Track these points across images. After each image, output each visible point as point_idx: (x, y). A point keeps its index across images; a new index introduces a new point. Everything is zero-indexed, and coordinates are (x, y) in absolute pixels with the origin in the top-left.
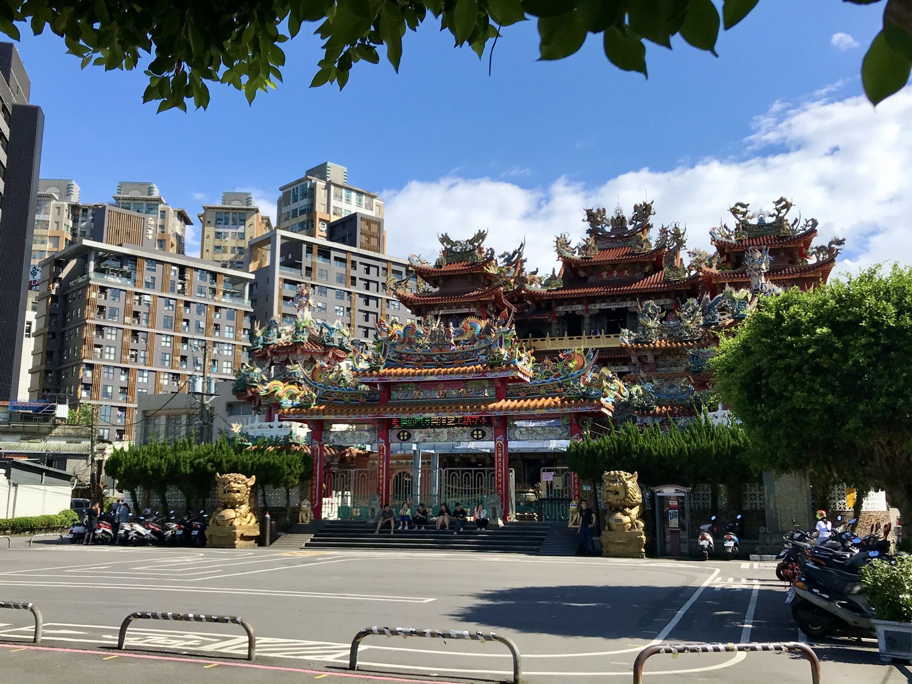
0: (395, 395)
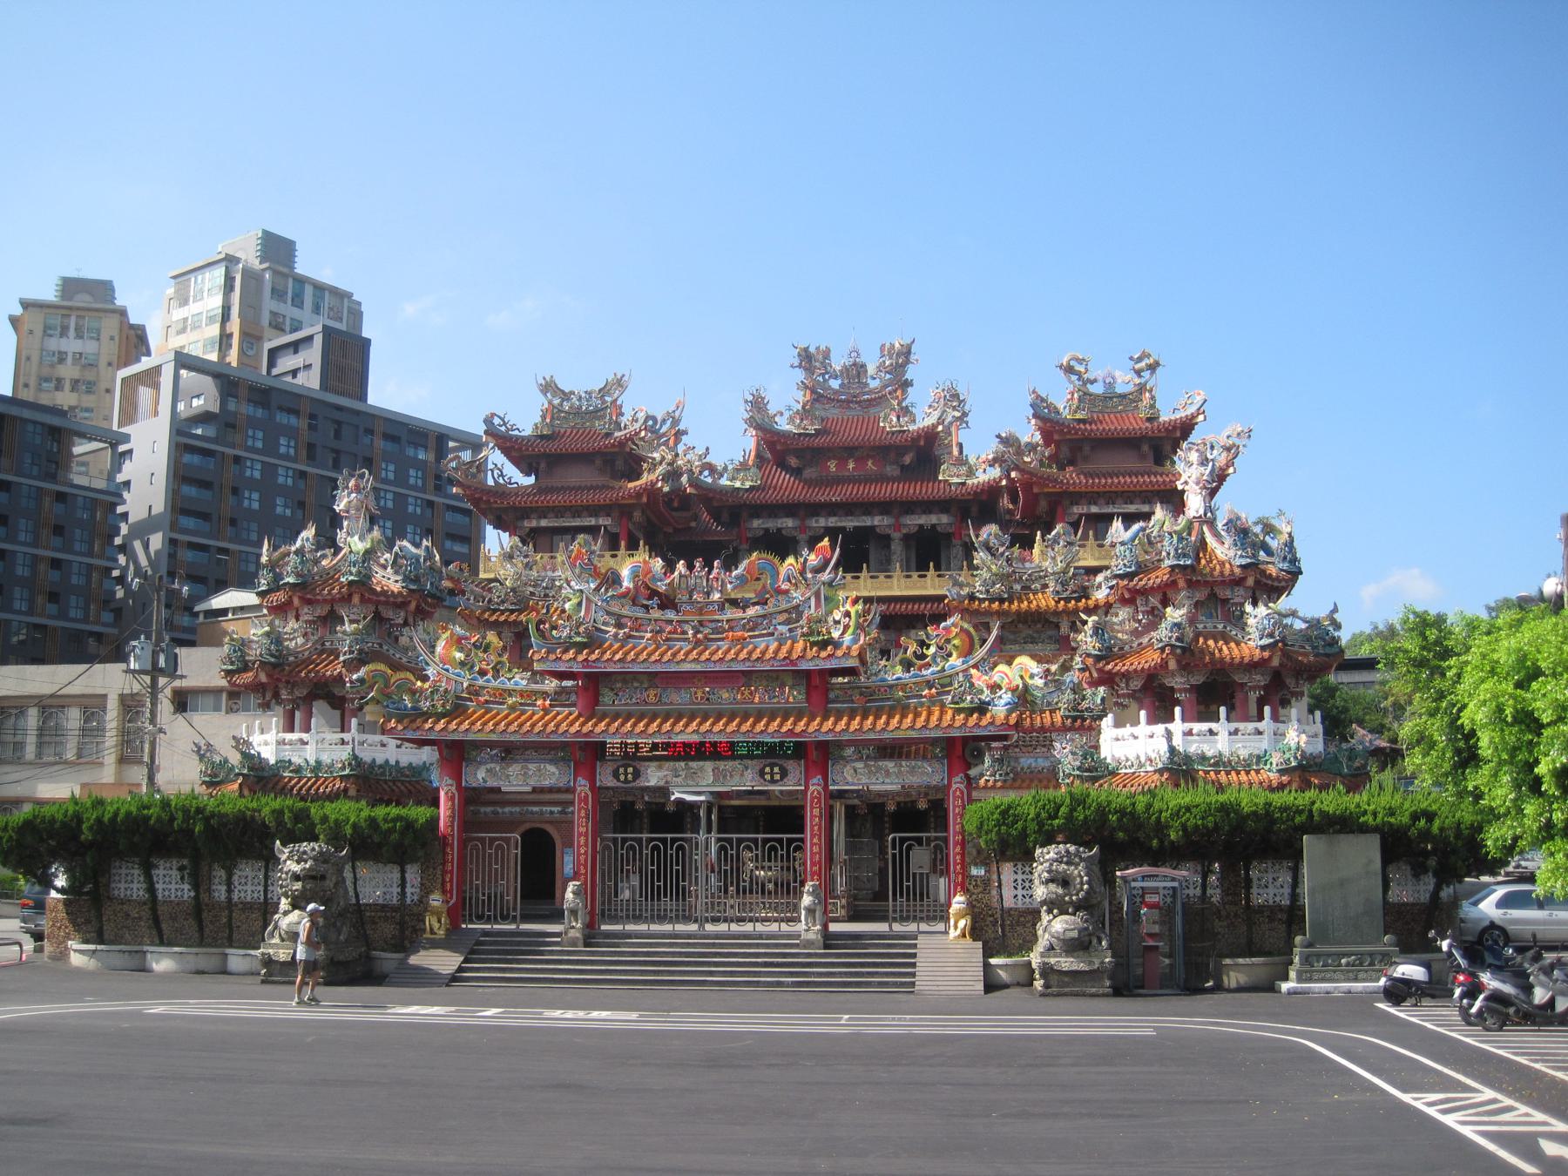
0: (607, 697)
